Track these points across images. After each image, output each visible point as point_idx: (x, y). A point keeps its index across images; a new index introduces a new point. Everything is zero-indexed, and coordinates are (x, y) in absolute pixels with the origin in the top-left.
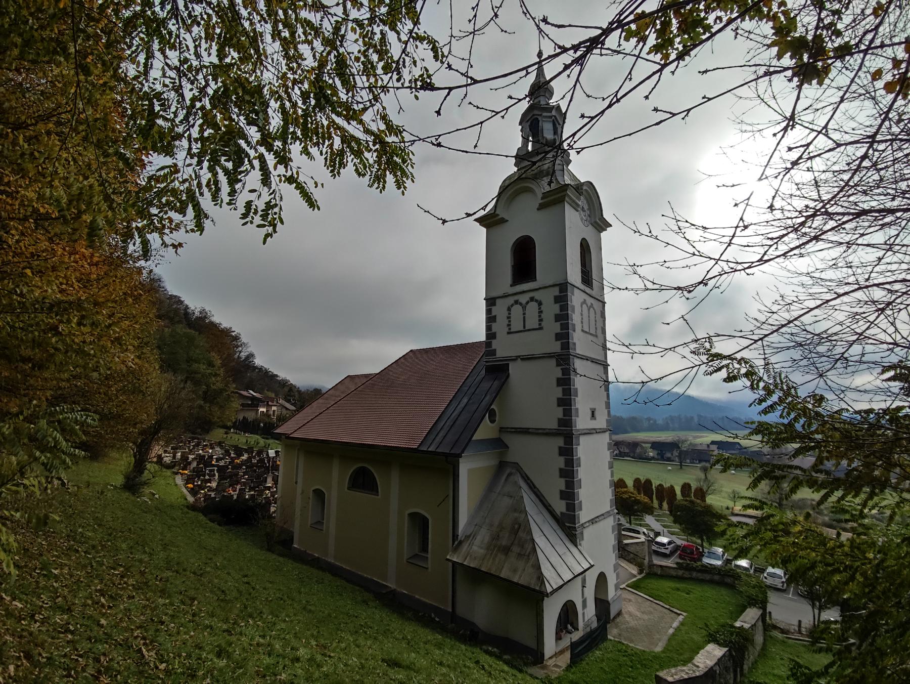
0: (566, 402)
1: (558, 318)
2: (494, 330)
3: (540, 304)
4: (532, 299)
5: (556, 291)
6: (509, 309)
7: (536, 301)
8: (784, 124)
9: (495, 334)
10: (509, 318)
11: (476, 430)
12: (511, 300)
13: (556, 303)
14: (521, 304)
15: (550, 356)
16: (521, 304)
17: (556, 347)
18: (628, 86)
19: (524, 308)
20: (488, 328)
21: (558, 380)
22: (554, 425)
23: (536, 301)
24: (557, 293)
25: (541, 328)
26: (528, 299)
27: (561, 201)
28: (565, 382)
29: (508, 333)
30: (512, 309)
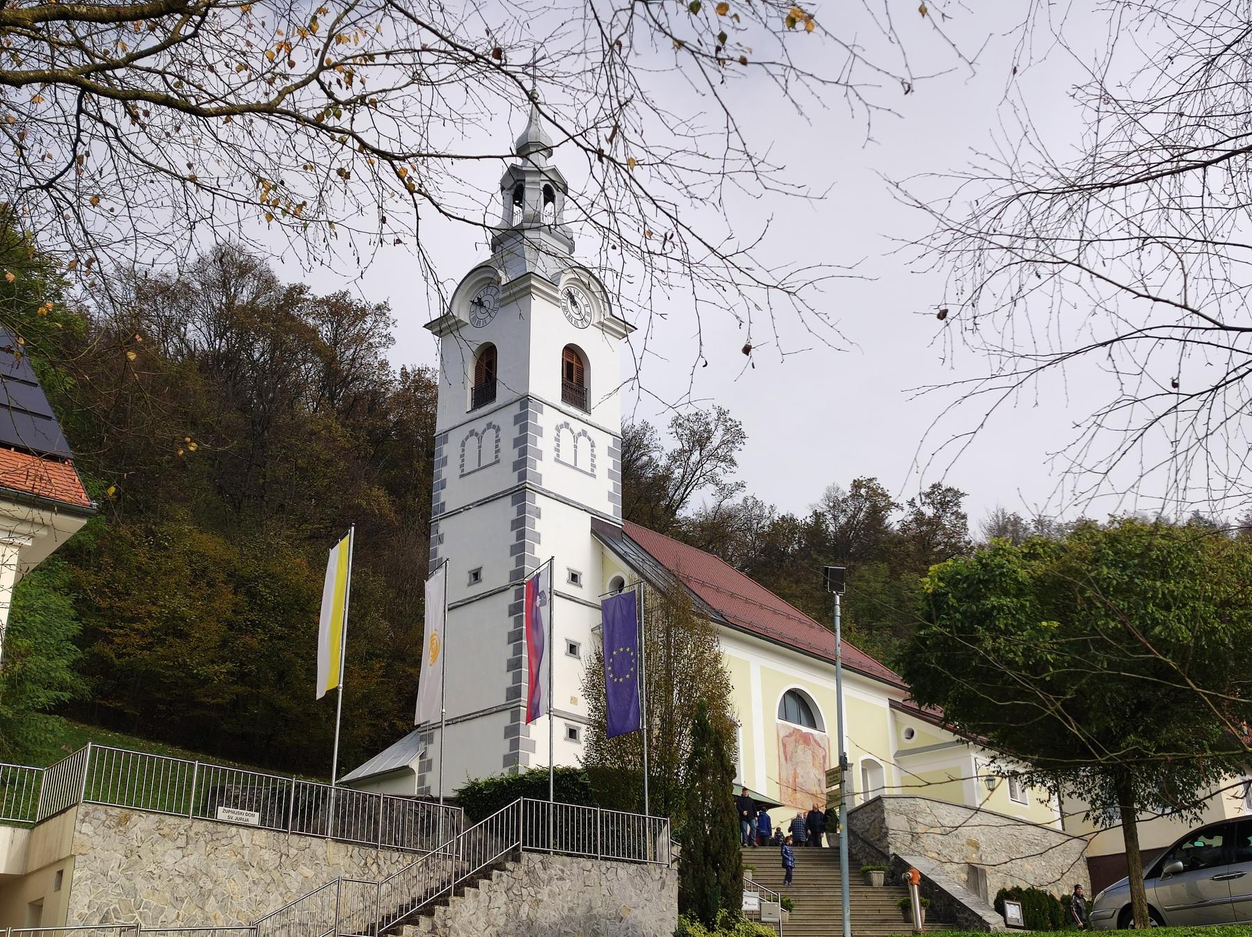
3: (498, 429)
4: (489, 426)
5: (515, 409)
6: (463, 444)
7: (494, 427)
8: (113, 112)
10: (462, 456)
12: (466, 430)
13: (512, 555)
14: (477, 434)
15: (504, 494)
16: (477, 434)
17: (512, 481)
18: (1006, 822)
22: (501, 700)
24: (518, 412)
25: (498, 462)
27: (527, 292)
29: (462, 476)
30: (467, 443)
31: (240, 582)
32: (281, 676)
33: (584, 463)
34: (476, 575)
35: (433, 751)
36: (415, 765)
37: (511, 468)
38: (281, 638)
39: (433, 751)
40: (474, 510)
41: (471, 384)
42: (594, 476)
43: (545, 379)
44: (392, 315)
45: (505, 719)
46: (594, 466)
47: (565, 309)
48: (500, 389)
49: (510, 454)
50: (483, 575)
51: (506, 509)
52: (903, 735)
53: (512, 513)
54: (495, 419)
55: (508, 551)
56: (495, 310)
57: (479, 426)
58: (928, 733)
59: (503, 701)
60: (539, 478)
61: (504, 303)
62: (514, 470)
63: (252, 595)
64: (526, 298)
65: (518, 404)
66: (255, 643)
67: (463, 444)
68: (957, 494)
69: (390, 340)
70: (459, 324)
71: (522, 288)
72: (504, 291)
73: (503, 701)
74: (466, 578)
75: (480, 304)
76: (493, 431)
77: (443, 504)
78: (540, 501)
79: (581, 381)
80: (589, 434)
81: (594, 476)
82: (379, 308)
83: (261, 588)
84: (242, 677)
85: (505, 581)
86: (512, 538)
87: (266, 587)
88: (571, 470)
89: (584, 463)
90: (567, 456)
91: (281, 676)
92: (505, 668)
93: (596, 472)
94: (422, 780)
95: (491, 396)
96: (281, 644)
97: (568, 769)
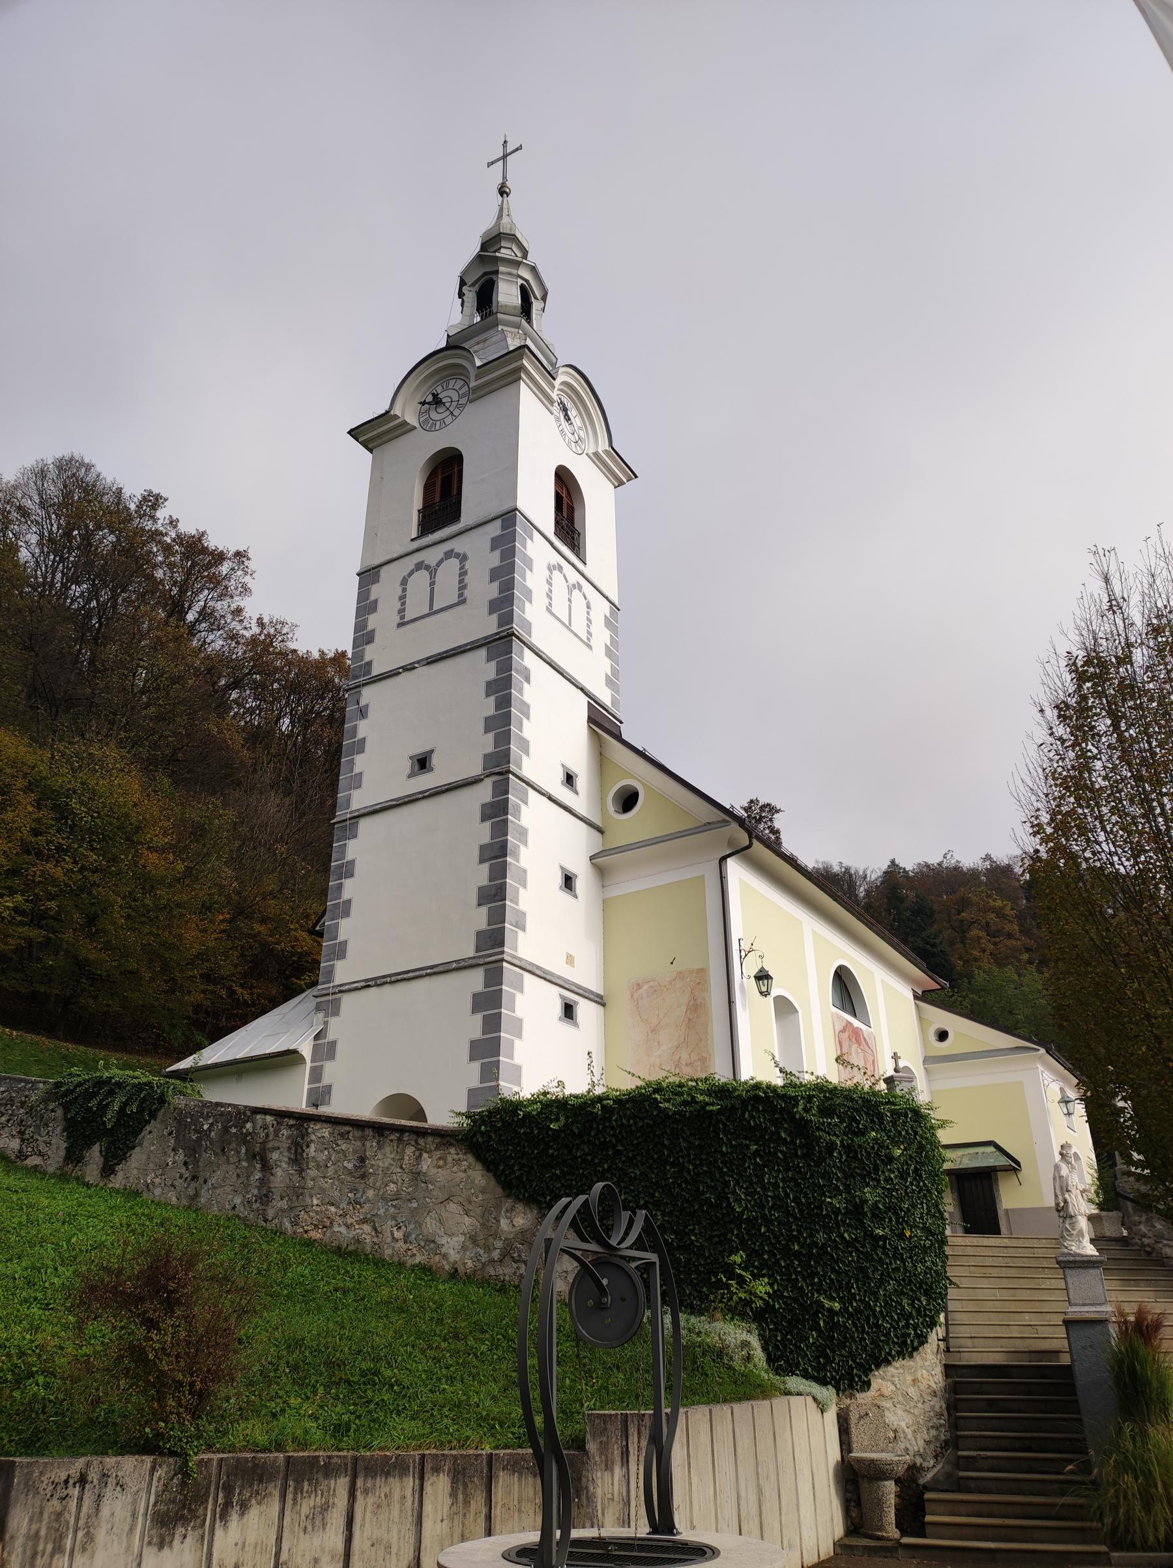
0: (501, 724)
1: (495, 574)
2: (326, 1080)
3: (463, 558)
6: (404, 582)
7: (457, 556)
9: (333, 1045)
11: (372, 420)
13: (472, 1058)
16: (427, 567)
17: (489, 626)
19: (433, 572)
20: (360, 626)
21: (474, 1044)
22: (467, 949)
23: (457, 556)
24: (498, 532)
25: (462, 601)
26: (441, 555)
27: (514, 377)
28: (501, 689)
29: (400, 625)
31: (45, 794)
32: (91, 920)
33: (579, 626)
34: (422, 763)
35: (337, 1028)
36: (306, 1050)
37: (486, 609)
38: (95, 871)
39: (337, 1028)
40: (422, 671)
41: (417, 503)
42: (590, 647)
43: (536, 502)
44: (252, 565)
45: (475, 980)
46: (589, 633)
47: (558, 419)
48: (462, 518)
49: (483, 590)
50: (435, 760)
51: (481, 667)
52: (932, 1038)
53: (490, 671)
54: (457, 545)
55: (481, 726)
56: (461, 407)
57: (432, 556)
58: (967, 1033)
59: (471, 952)
60: (528, 626)
61: (476, 395)
62: (491, 612)
63: (63, 813)
64: (512, 387)
65: (498, 523)
66: (59, 873)
67: (404, 582)
68: (772, 810)
69: (246, 590)
70: (404, 428)
71: (506, 371)
72: (478, 377)
73: (471, 952)
74: (407, 766)
75: (437, 401)
76: (454, 562)
77: (369, 664)
78: (529, 660)
79: (571, 519)
80: (584, 589)
81: (590, 647)
82: (238, 554)
83: (74, 803)
84: (37, 918)
85: (476, 769)
86: (489, 707)
87: (82, 803)
88: (562, 627)
89: (579, 626)
90: (561, 610)
91: (91, 920)
92: (475, 901)
93: (592, 643)
94: (316, 1074)
95: (453, 513)
96: (96, 878)
97: (757, 1086)
